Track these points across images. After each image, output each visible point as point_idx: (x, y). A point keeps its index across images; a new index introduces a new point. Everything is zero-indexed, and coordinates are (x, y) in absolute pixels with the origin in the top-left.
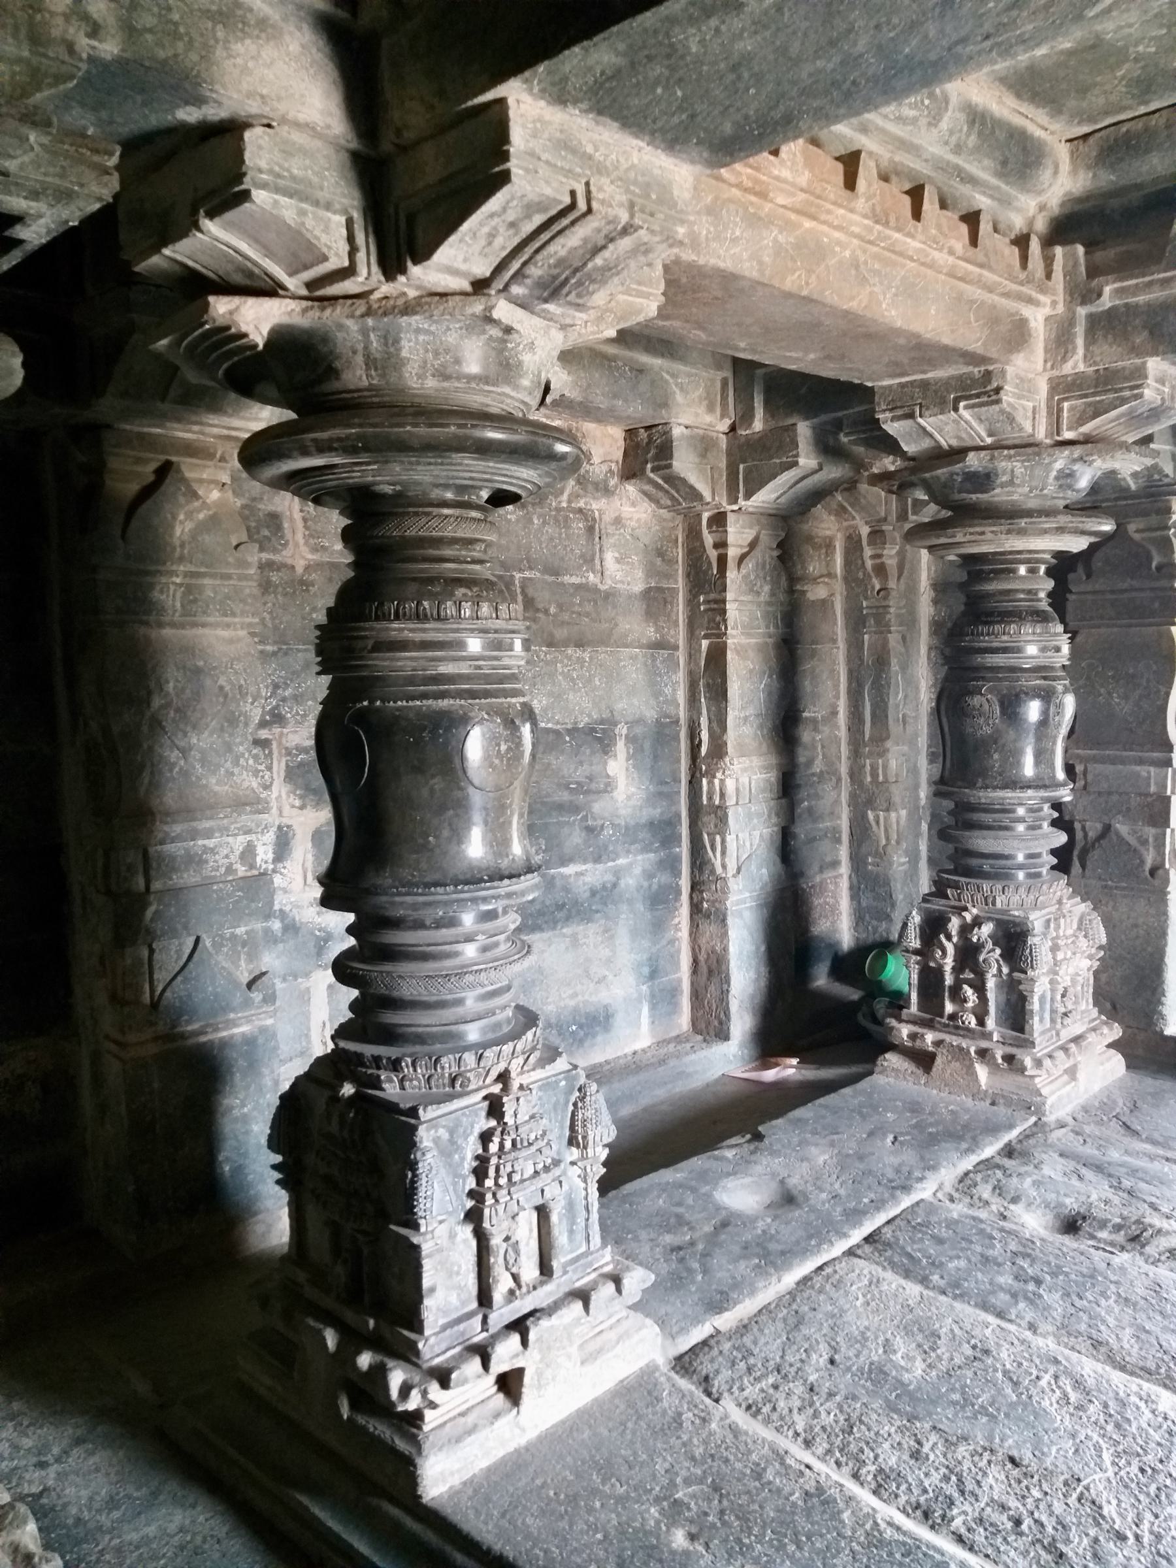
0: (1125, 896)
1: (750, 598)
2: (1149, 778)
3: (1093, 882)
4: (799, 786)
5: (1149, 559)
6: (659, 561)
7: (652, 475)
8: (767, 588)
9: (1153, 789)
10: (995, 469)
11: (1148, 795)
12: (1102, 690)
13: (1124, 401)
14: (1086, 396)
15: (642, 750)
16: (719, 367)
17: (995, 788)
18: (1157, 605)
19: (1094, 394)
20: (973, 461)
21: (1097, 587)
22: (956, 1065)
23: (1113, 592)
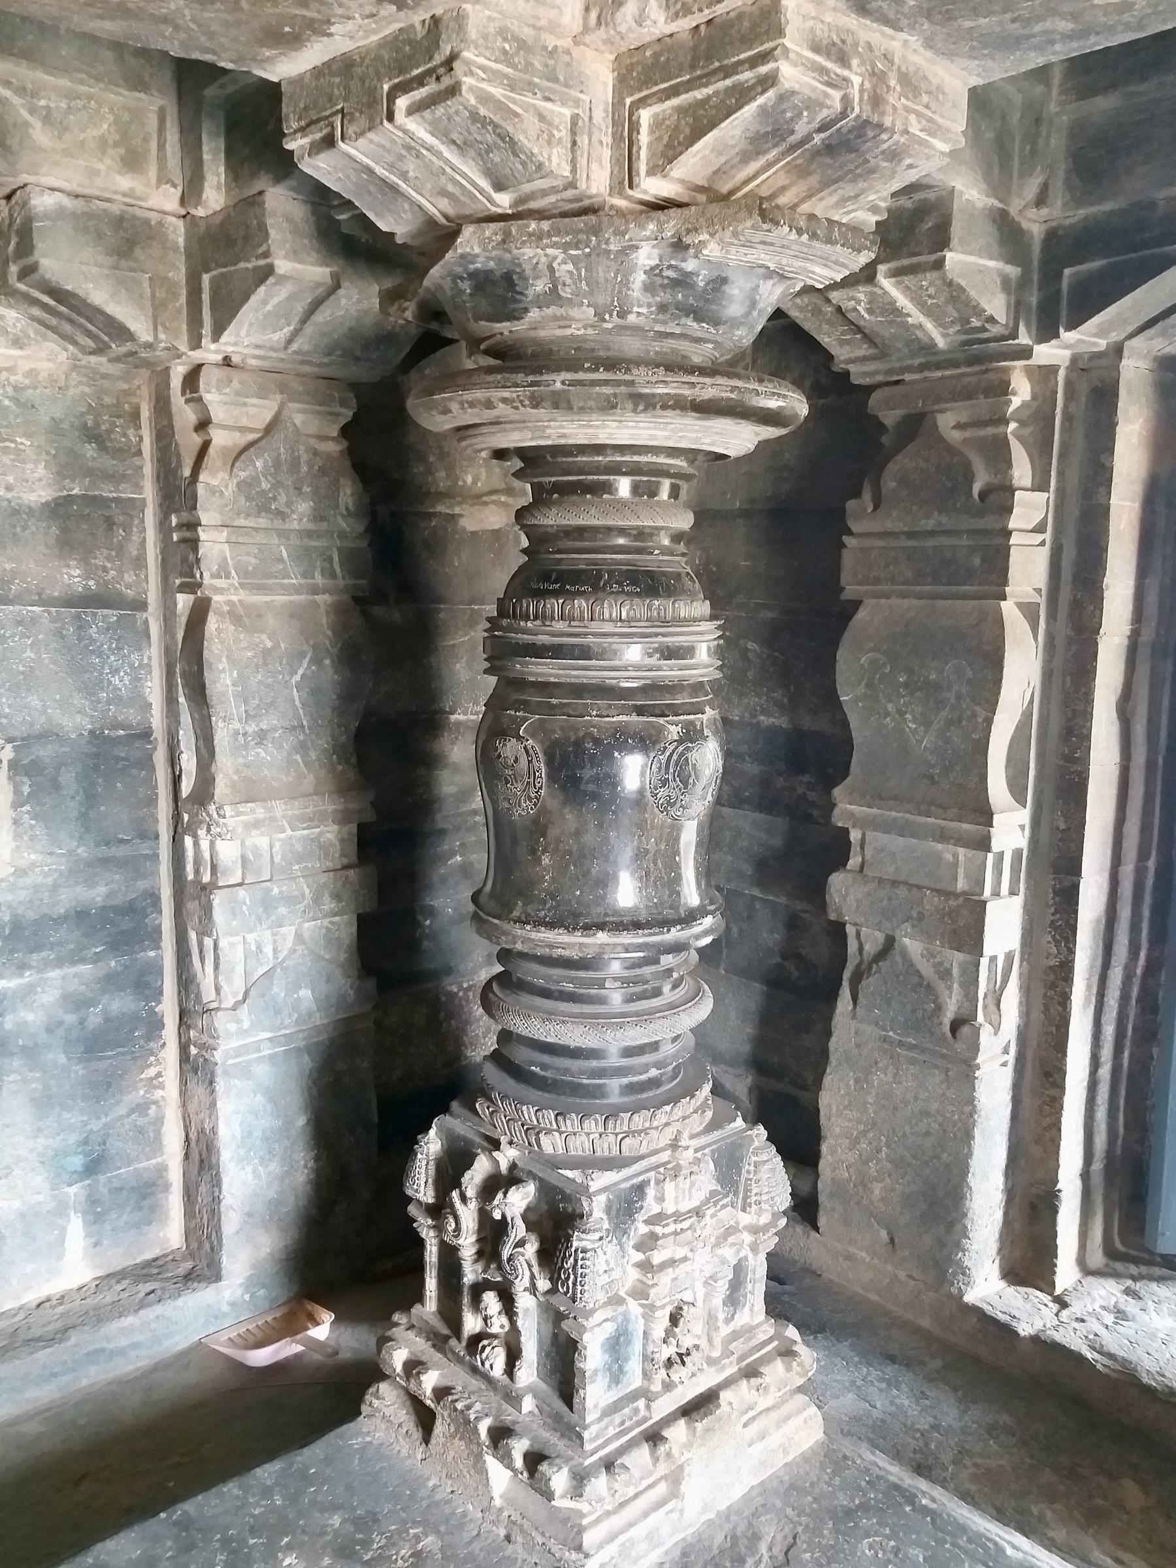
0: (913, 1062)
1: (263, 522)
2: (955, 864)
3: (869, 1029)
4: (442, 833)
5: (970, 478)
6: (90, 450)
7: (21, 286)
8: (304, 507)
9: (961, 884)
10: (516, 262)
11: (950, 894)
13: (743, 95)
14: (674, 92)
15: (56, 786)
16: (138, 84)
18: (977, 561)
19: (689, 86)
20: (472, 244)
21: (889, 525)
23: (911, 535)
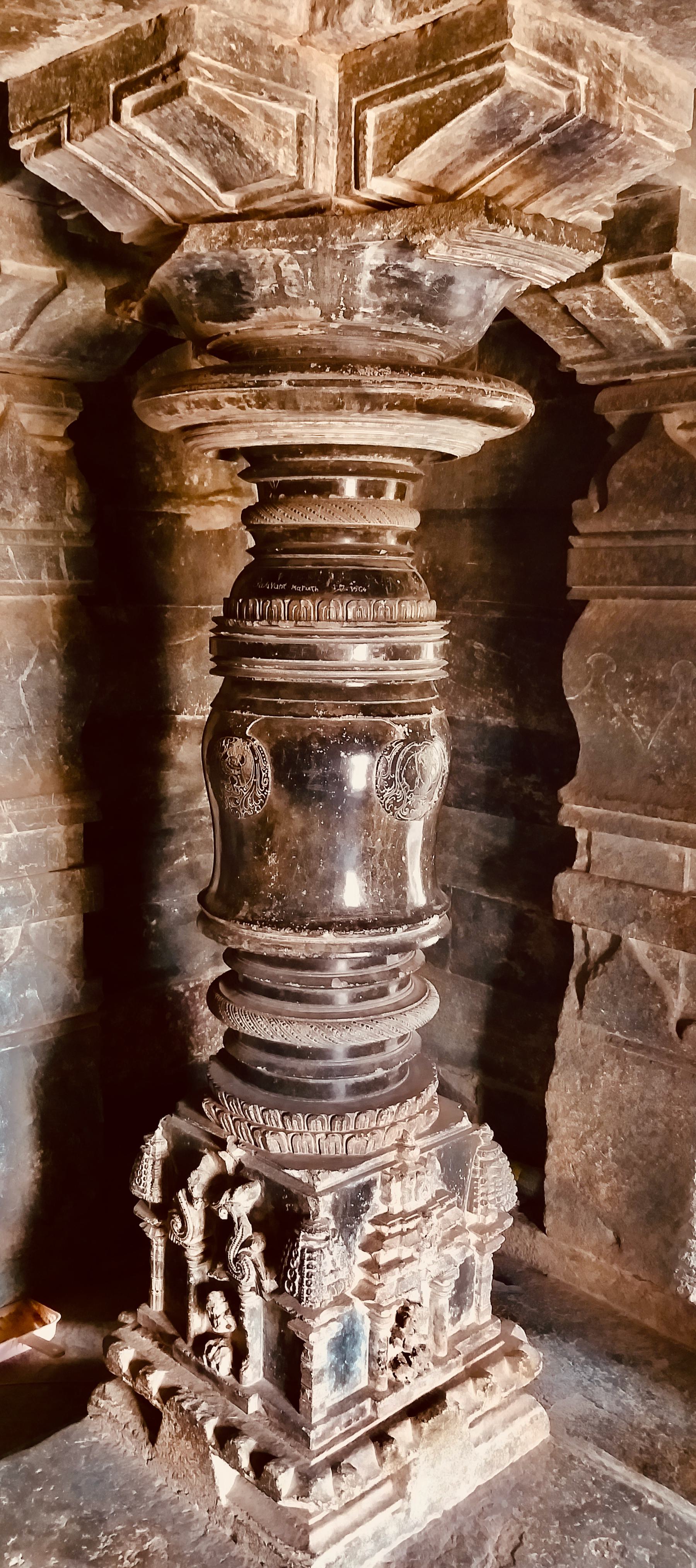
0: (639, 1062)
2: (682, 865)
3: (595, 1029)
4: (169, 833)
11: (680, 895)
12: (616, 707)
13: (468, 96)
14: (400, 92)
17: (266, 923)
19: (415, 86)
21: (615, 525)
22: (185, 1444)
23: (637, 535)
